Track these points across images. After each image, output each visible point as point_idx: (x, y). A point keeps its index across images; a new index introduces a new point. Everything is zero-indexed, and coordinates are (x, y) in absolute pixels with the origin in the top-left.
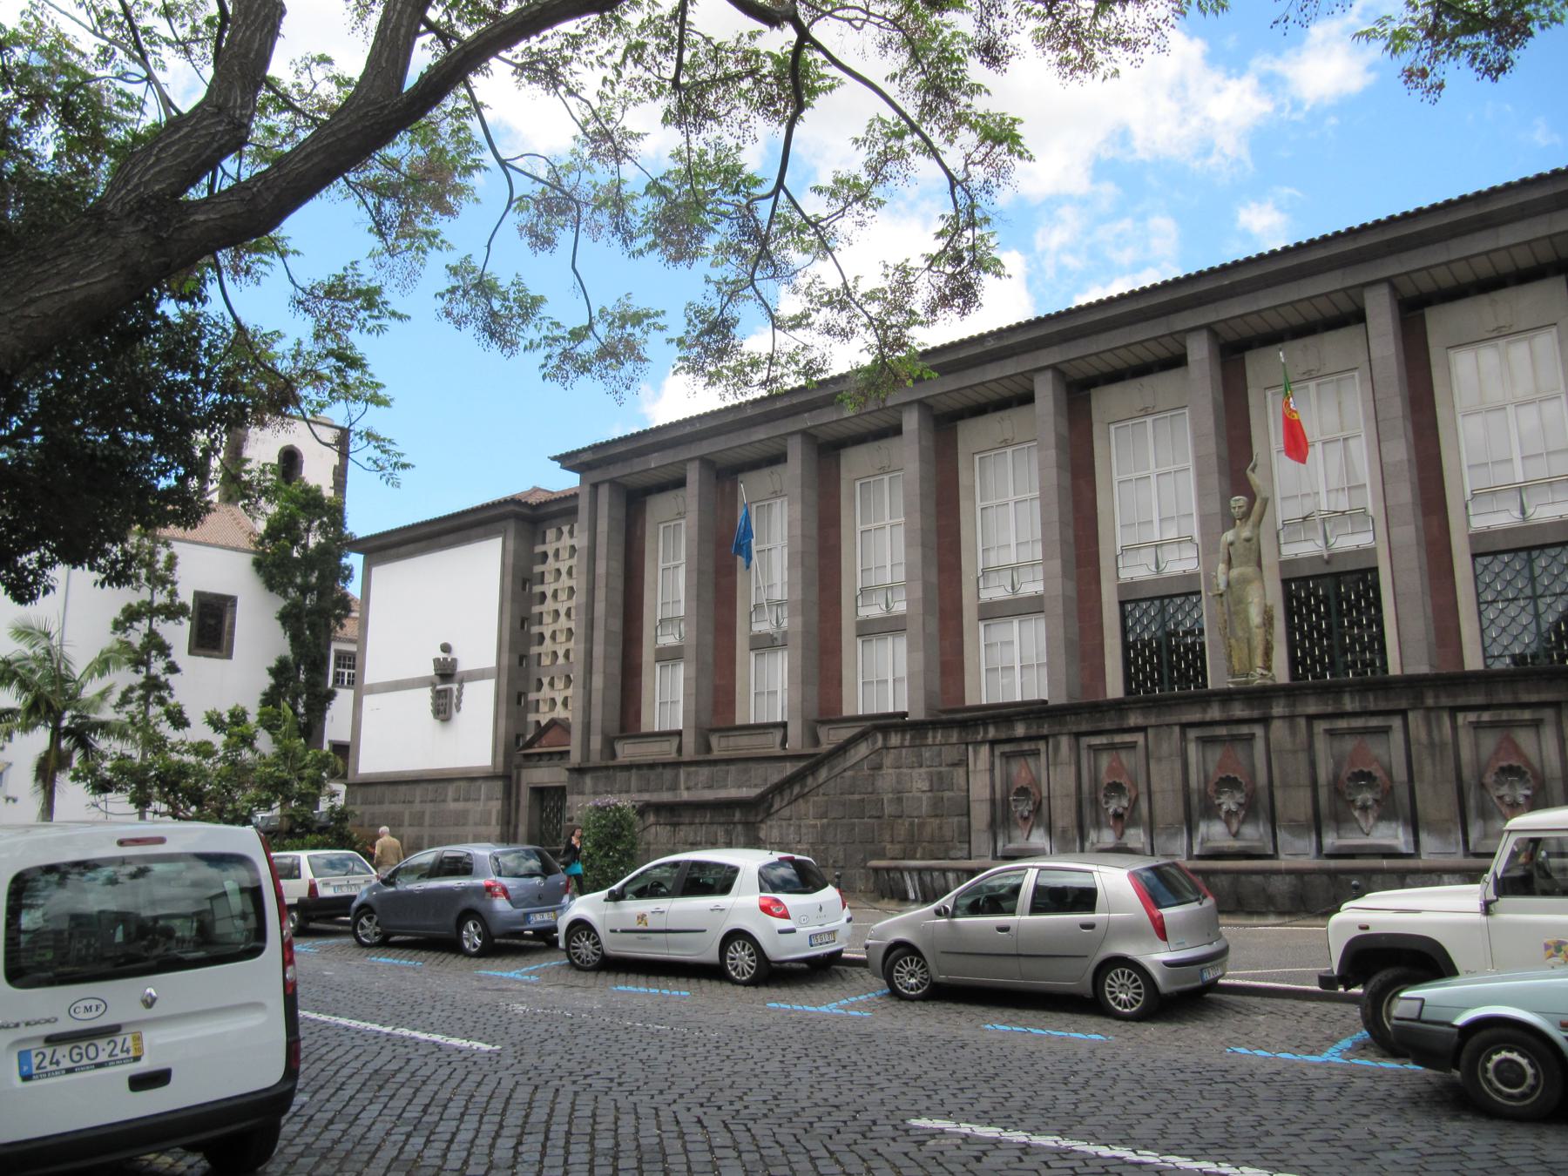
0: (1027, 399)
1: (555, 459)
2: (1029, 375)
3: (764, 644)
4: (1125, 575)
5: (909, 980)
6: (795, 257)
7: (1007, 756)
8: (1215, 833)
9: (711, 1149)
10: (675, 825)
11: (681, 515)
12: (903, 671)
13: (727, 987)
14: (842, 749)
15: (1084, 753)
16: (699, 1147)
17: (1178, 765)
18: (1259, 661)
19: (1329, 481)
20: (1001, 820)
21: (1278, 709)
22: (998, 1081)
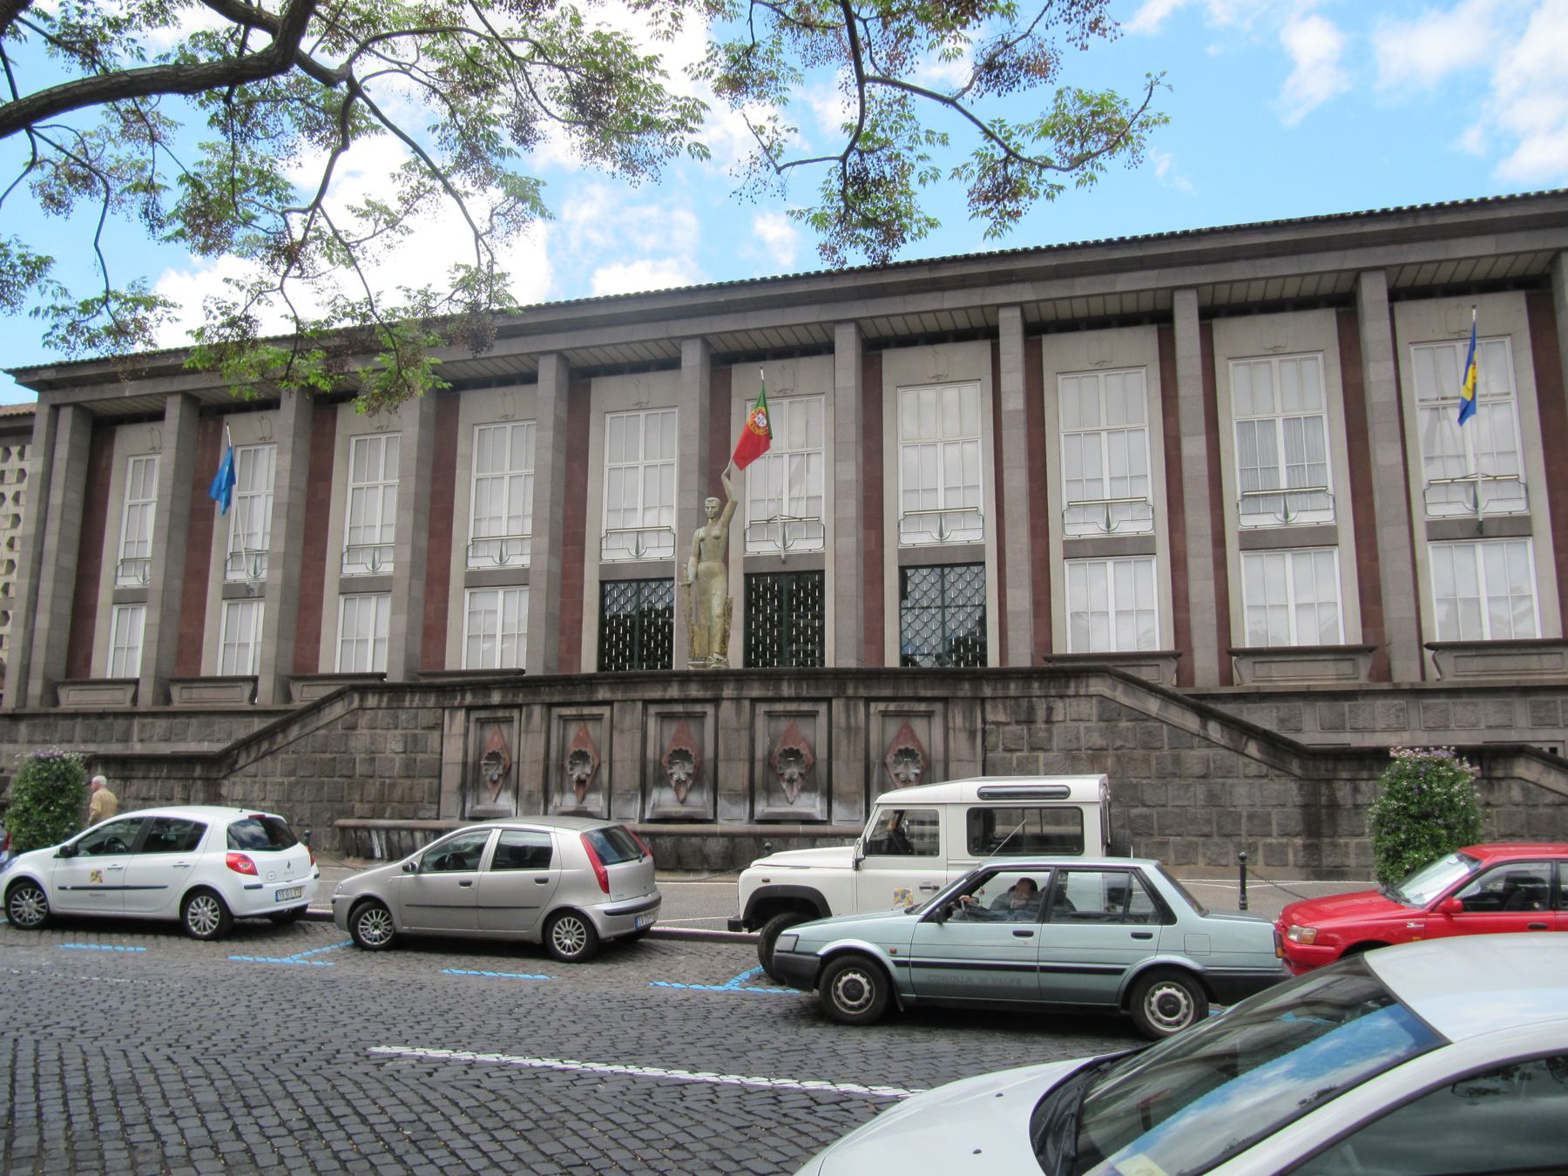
0: (530, 378)
1: (9, 372)
2: (536, 356)
3: (238, 594)
4: (608, 557)
5: (373, 931)
6: (322, 263)
7: (482, 723)
8: (665, 800)
9: (184, 1080)
10: (126, 779)
11: (155, 450)
12: (384, 632)
13: (187, 942)
14: (317, 707)
15: (554, 723)
16: (171, 1078)
17: (638, 736)
18: (716, 647)
19: (791, 497)
20: (471, 782)
21: (728, 692)
22: (451, 1015)
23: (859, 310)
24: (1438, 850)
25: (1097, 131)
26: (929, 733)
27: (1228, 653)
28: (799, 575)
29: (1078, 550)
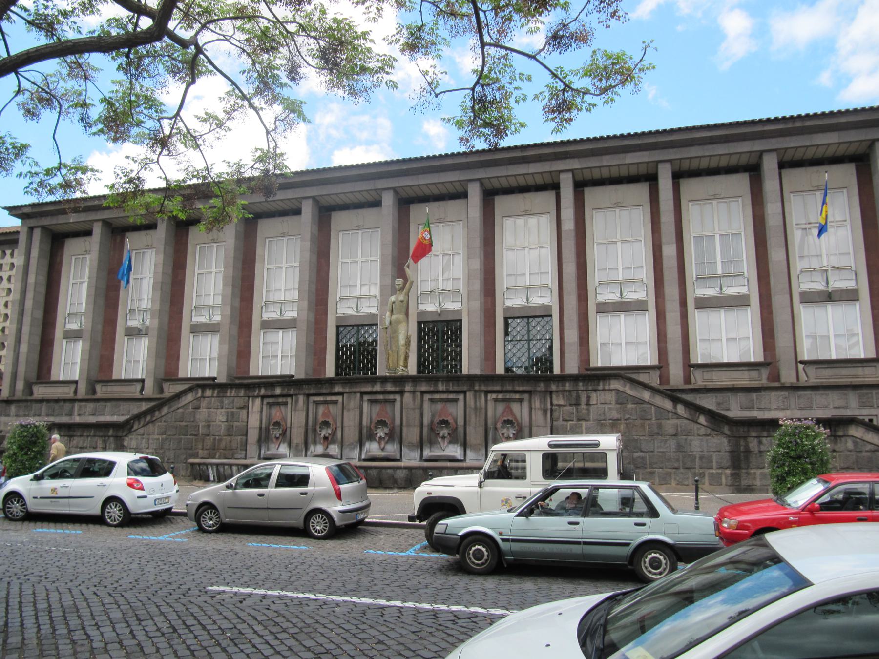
0: (297, 212)
1: (5, 208)
2: (300, 200)
3: (133, 333)
4: (341, 312)
5: (209, 522)
6: (181, 147)
7: (270, 405)
8: (373, 448)
9: (103, 605)
10: (71, 437)
11: (87, 252)
12: (215, 354)
13: (105, 528)
14: (178, 396)
15: (311, 405)
16: (96, 604)
17: (358, 413)
18: (401, 363)
19: (443, 278)
20: (264, 438)
21: (408, 388)
22: (253, 569)
23: (482, 174)
24: (806, 476)
25: (615, 73)
26: (521, 411)
27: (689, 366)
28: (448, 322)
29: (604, 308)
